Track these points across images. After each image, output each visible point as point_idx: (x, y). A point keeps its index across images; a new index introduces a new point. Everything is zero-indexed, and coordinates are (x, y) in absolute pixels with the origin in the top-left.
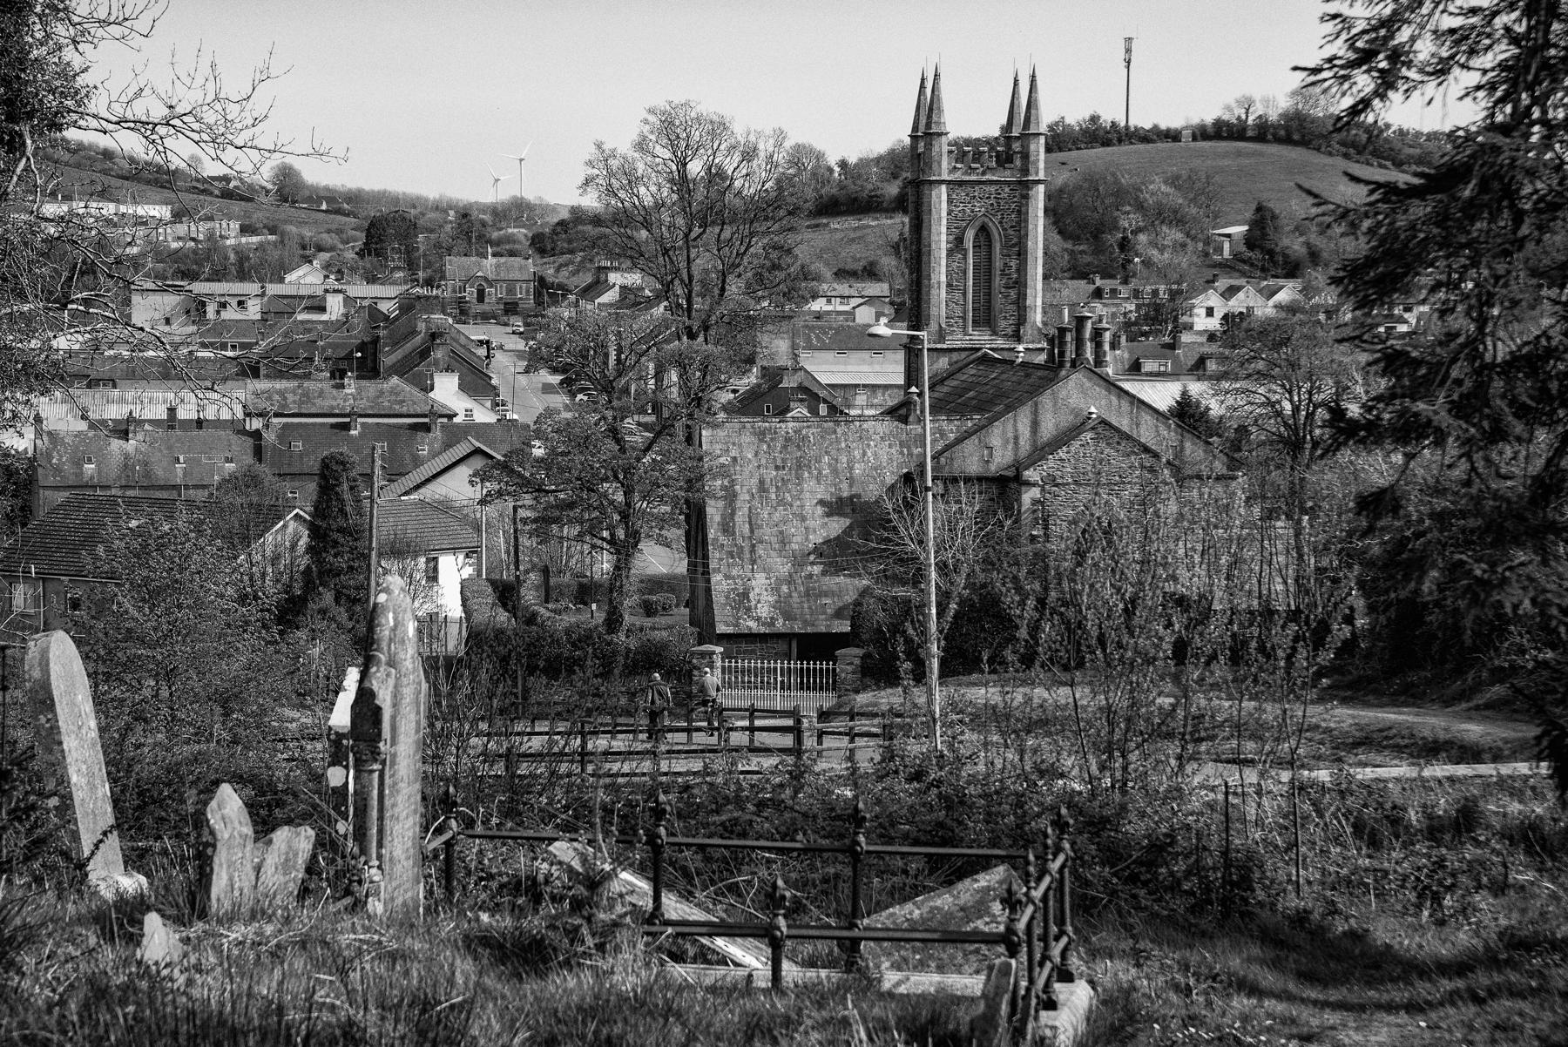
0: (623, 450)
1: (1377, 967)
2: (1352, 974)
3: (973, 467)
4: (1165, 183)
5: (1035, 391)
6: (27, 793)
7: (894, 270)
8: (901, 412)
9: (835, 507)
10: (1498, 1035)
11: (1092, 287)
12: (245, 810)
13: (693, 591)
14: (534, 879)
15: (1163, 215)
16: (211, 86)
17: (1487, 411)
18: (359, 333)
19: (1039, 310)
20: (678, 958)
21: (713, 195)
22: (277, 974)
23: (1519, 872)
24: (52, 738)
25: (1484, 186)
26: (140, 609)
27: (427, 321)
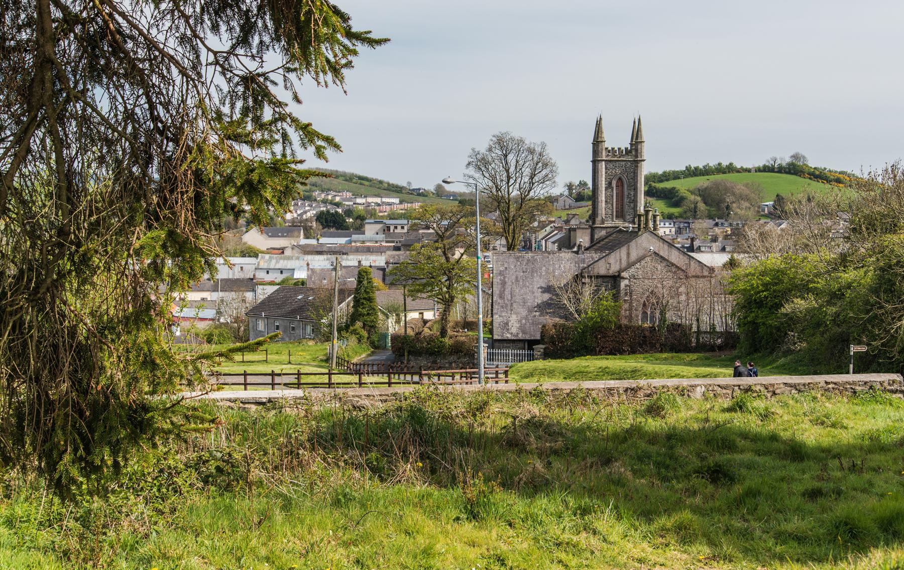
3: (603, 272)
15: (742, 197)
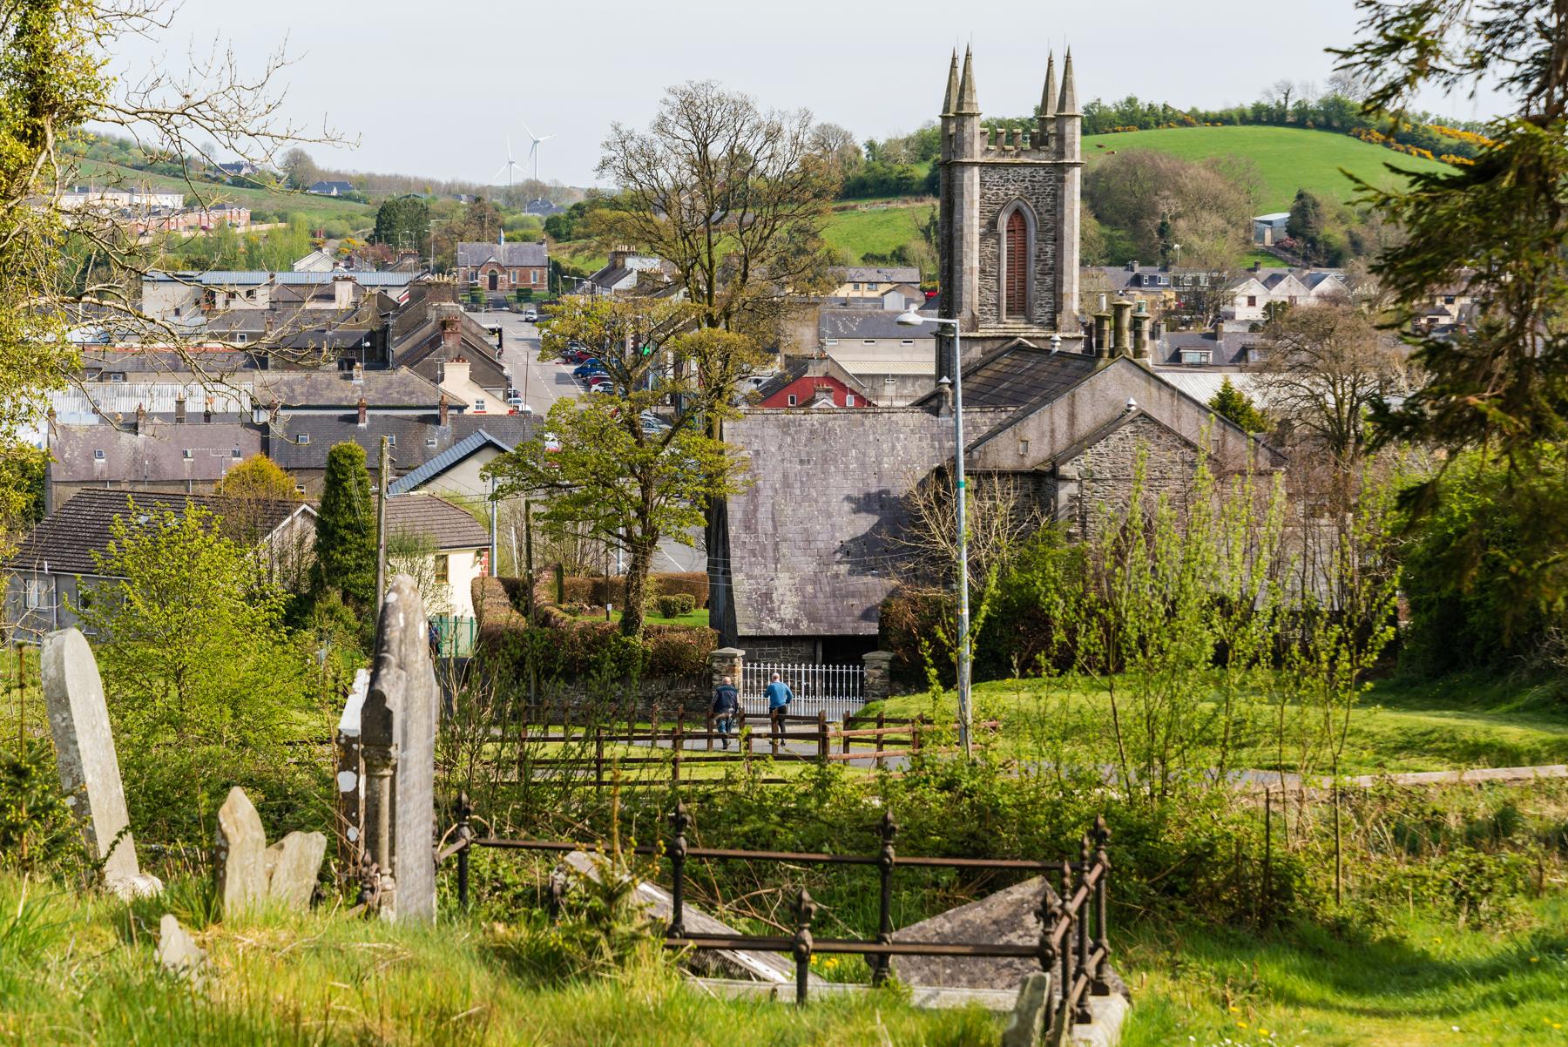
0: (640, 443)
1: (1414, 973)
2: (1389, 981)
3: (1008, 462)
4: (1205, 167)
5: (1073, 381)
6: (44, 792)
7: (924, 256)
8: (931, 404)
9: (865, 503)
10: (1528, 1036)
11: (1130, 275)
12: (257, 815)
13: (713, 590)
14: (550, 891)
16: (226, 75)
17: (1527, 407)
18: (368, 322)
19: (1076, 298)
20: (698, 971)
21: (735, 177)
22: (293, 978)
23: (1552, 875)
24: (67, 736)
25: (1521, 178)
26: (150, 608)
27: (438, 309)
